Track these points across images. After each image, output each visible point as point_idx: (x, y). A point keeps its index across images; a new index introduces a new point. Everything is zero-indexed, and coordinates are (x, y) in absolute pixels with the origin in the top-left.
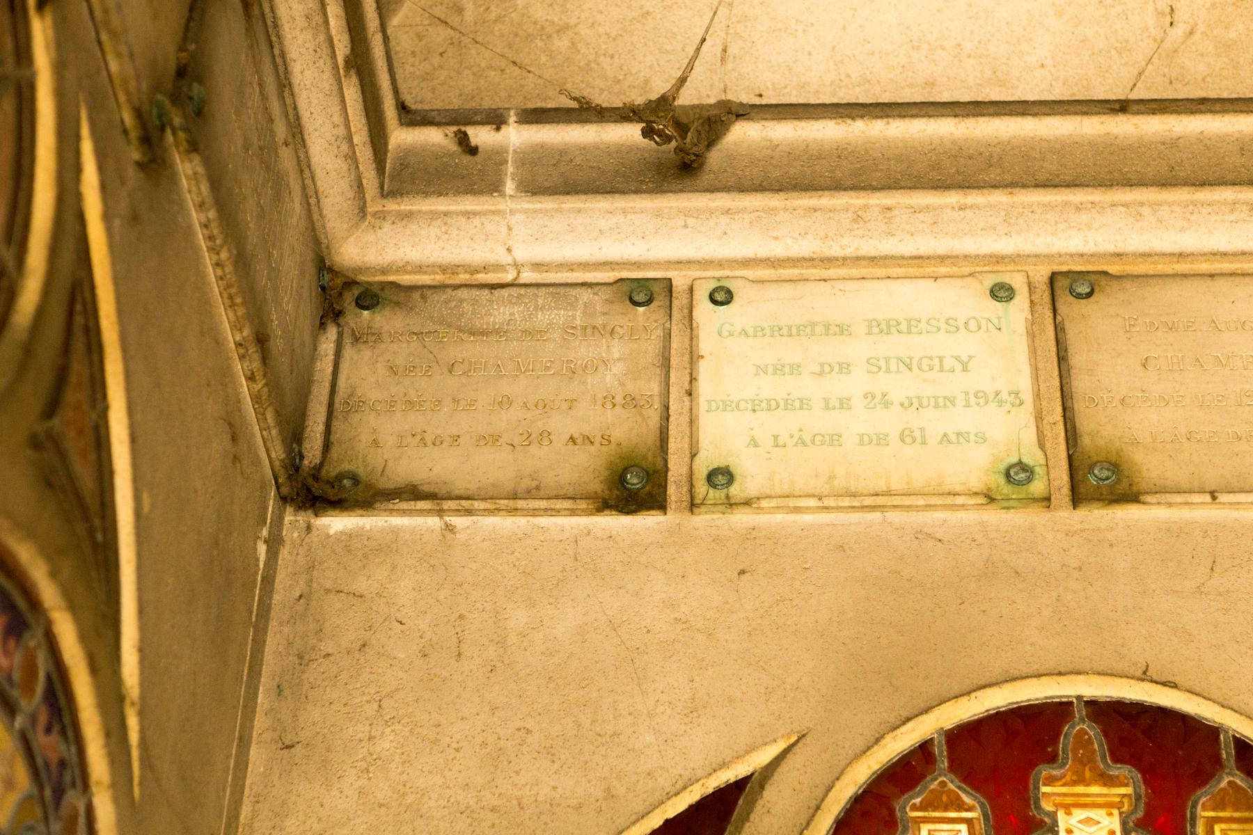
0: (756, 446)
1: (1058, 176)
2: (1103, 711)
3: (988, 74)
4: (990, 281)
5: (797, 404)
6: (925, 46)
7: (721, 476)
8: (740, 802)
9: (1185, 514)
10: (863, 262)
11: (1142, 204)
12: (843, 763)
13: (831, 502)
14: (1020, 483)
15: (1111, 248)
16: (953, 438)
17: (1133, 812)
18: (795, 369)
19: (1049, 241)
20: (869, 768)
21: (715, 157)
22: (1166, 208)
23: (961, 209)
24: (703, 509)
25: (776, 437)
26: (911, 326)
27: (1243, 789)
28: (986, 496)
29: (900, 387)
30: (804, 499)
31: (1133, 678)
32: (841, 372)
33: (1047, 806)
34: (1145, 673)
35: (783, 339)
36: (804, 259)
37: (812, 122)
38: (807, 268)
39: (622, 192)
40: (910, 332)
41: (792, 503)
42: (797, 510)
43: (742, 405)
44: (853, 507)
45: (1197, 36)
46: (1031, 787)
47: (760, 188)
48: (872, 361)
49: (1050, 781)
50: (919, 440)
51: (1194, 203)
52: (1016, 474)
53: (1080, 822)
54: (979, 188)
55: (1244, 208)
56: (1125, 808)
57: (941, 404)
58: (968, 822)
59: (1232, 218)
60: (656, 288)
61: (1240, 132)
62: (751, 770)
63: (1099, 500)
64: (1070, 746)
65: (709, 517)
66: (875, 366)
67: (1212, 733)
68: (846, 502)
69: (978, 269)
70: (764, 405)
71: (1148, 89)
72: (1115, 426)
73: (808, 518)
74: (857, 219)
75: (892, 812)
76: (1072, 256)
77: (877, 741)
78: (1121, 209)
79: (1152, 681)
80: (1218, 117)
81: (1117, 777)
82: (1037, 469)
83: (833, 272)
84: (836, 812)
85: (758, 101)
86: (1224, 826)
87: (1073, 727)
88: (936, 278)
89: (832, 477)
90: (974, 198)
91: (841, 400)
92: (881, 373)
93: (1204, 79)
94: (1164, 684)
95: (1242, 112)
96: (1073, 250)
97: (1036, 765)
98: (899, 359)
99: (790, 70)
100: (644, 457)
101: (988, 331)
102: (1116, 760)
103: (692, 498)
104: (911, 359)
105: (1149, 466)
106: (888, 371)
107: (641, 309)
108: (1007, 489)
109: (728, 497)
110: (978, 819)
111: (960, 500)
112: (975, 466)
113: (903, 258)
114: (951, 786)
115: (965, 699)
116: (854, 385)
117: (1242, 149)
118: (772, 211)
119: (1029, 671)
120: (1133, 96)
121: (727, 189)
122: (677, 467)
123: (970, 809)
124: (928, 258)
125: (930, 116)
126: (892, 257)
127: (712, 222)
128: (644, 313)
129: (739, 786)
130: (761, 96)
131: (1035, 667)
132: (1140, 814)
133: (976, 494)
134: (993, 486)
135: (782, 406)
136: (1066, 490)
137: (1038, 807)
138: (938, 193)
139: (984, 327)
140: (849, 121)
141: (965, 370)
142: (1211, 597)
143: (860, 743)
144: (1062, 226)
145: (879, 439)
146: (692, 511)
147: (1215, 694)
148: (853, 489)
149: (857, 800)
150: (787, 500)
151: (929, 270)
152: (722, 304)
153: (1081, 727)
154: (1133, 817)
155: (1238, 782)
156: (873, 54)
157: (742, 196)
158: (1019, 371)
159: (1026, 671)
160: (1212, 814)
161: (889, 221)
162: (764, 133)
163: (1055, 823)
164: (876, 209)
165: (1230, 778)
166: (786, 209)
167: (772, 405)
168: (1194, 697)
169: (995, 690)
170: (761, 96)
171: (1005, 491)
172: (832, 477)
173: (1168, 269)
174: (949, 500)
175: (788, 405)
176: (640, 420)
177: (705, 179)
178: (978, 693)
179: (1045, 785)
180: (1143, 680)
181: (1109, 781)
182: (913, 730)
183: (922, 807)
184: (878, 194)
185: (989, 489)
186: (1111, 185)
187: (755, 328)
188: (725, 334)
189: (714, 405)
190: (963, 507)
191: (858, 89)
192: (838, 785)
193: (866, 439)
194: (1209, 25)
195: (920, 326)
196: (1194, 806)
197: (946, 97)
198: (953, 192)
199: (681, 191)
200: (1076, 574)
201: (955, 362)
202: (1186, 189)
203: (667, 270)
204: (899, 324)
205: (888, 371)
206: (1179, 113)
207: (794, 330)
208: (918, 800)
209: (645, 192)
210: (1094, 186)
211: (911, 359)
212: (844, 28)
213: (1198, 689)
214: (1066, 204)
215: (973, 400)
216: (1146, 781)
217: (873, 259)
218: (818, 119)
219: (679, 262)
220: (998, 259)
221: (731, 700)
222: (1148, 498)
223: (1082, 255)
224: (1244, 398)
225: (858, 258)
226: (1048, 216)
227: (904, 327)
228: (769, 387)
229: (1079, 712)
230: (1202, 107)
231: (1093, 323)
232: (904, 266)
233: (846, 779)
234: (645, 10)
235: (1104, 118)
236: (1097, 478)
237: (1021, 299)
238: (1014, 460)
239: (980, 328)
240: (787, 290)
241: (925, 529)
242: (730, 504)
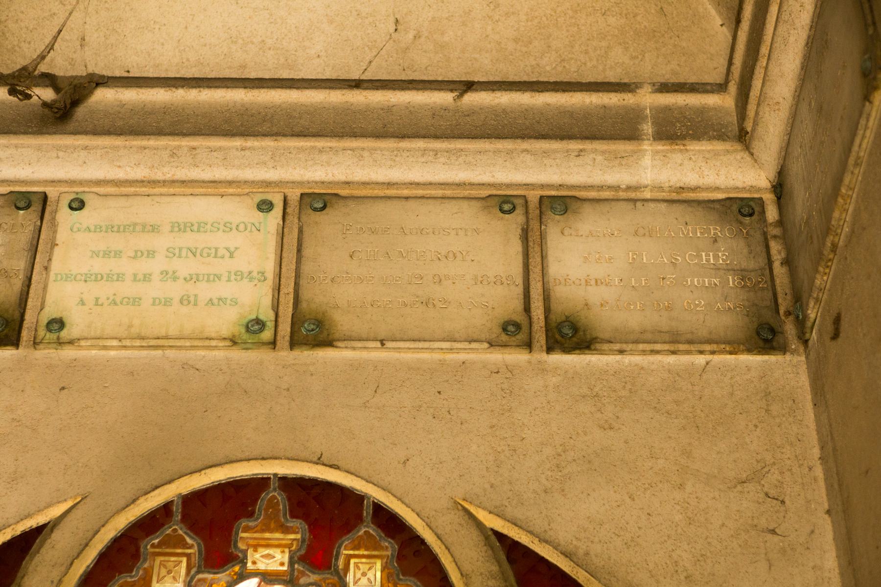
0: (83, 304)
1: (308, 129)
2: (289, 484)
3: (282, 60)
4: (258, 198)
5: (115, 277)
6: (240, 41)
7: (58, 324)
8: (38, 541)
9: (364, 354)
10: (177, 184)
11: (363, 149)
12: (108, 516)
13: (128, 343)
14: (254, 332)
15: (343, 178)
16: (215, 301)
17: (299, 550)
18: (118, 254)
19: (302, 172)
20: (127, 519)
21: (81, 111)
22: (379, 152)
23: (242, 150)
24: (41, 346)
25: (97, 299)
26: (199, 227)
27: (372, 535)
28: (231, 340)
29: (185, 267)
30: (110, 341)
31: (311, 462)
32: (148, 257)
33: (241, 546)
34: (319, 459)
35: (114, 234)
36: (137, 181)
37: (149, 90)
38: (140, 187)
39: (15, 133)
40: (198, 231)
41: (101, 343)
42: (105, 348)
43: (79, 277)
44: (142, 347)
45: (423, 39)
46: (234, 533)
47: (108, 132)
48: (171, 250)
49: (247, 529)
50: (192, 303)
51: (398, 149)
52: (253, 326)
53: (262, 556)
54: (254, 136)
55: (431, 153)
56: (294, 548)
57: (211, 279)
58: (188, 556)
59: (423, 160)
60: (517, 201)
61: (435, 103)
62: (48, 520)
63: (306, 344)
64: (264, 506)
65: (47, 351)
66: (171, 253)
67: (359, 499)
68: (138, 343)
69: (254, 190)
70: (93, 277)
71: (389, 73)
72: (325, 296)
73: (112, 353)
74: (173, 155)
75: (138, 550)
76: (316, 183)
77: (134, 501)
78: (349, 152)
79: (324, 465)
80: (420, 93)
81: (292, 527)
82: (268, 324)
83: (157, 190)
84: (100, 548)
85: (126, 75)
86: (357, 560)
87: (267, 494)
88: (222, 196)
89: (130, 326)
90: (251, 142)
91: (145, 275)
92: (175, 258)
93: (426, 68)
94: (331, 466)
95: (436, 89)
96: (317, 179)
97: (239, 519)
98: (189, 249)
99: (149, 55)
100: (7, 311)
101: (251, 231)
102: (293, 516)
103: (35, 338)
104: (196, 249)
105: (343, 322)
106: (180, 257)
107: (22, 212)
108: (246, 337)
109: (58, 338)
110: (195, 554)
111: (214, 343)
112: (227, 321)
113: (203, 182)
114: (180, 532)
115: (197, 474)
116: (155, 266)
117: (434, 114)
118: (116, 148)
119: (243, 456)
120: (363, 77)
121: (85, 133)
122: (30, 317)
123: (191, 547)
124: (220, 182)
125: (228, 88)
126: (196, 181)
127: (75, 155)
128: (23, 214)
129: (39, 531)
130: (128, 72)
131: (247, 454)
132: (303, 552)
133: (225, 339)
134: (237, 334)
135: (105, 278)
136: (288, 338)
137: (236, 546)
138: (227, 139)
139: (249, 229)
140: (174, 89)
141: (231, 256)
142: (373, 410)
143: (122, 503)
144: (310, 163)
145: (166, 302)
146: (35, 348)
147: (364, 473)
148: (143, 334)
149: (116, 541)
150: (98, 340)
151: (222, 190)
152: (76, 209)
153: (275, 494)
154: (298, 554)
155: (371, 531)
156: (205, 45)
157: (96, 137)
158: (267, 258)
159: (240, 456)
160: (351, 552)
161: (194, 157)
162: (117, 96)
163: (246, 557)
164: (186, 149)
165: (367, 528)
166: (125, 147)
167: (98, 278)
168: (349, 475)
169: (219, 469)
170: (128, 72)
171: (244, 338)
172: (130, 326)
173: (381, 193)
174: (207, 343)
175: (109, 277)
176: (8, 285)
177: (72, 125)
178: (207, 471)
179: (242, 532)
180: (317, 464)
181: (286, 530)
182: (160, 494)
183: (159, 545)
184: (187, 139)
185: (234, 336)
186: (342, 136)
187: (96, 226)
188: (75, 229)
189: (59, 277)
190: (216, 347)
191: (194, 69)
192: (103, 530)
193: (157, 301)
194: (430, 32)
195: (207, 227)
196: (340, 547)
197: (253, 75)
198: (237, 138)
199: (55, 133)
200: (285, 393)
201: (225, 251)
202: (392, 140)
203: (45, 186)
204: (192, 225)
205: (180, 257)
206: (394, 89)
207: (122, 229)
208: (156, 541)
209: (30, 133)
210: (331, 136)
211: (196, 249)
212: (186, 28)
213: (352, 470)
214: (313, 148)
215: (233, 277)
216: (311, 531)
217: (183, 182)
218: (152, 87)
219: (53, 182)
220: (267, 184)
221: (41, 473)
222: (339, 344)
223: (323, 183)
224: (414, 280)
225: (173, 182)
226: (301, 156)
227: (195, 228)
228: (99, 266)
229: (274, 484)
230: (410, 86)
231: (326, 227)
232: (205, 187)
233: (109, 526)
234: (52, 12)
235: (344, 91)
236: (311, 330)
237: (278, 211)
238: (254, 317)
239: (246, 229)
240: (122, 201)
241: (190, 363)
242: (60, 343)
